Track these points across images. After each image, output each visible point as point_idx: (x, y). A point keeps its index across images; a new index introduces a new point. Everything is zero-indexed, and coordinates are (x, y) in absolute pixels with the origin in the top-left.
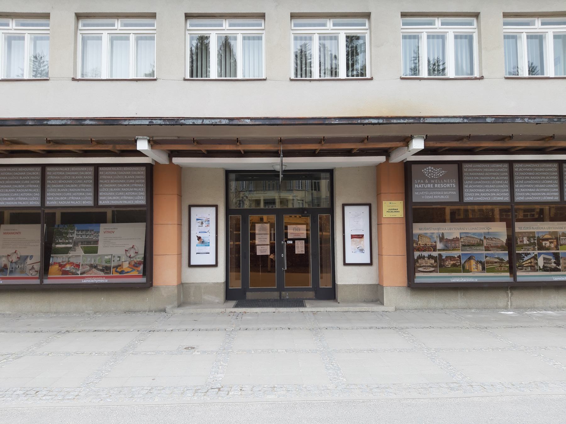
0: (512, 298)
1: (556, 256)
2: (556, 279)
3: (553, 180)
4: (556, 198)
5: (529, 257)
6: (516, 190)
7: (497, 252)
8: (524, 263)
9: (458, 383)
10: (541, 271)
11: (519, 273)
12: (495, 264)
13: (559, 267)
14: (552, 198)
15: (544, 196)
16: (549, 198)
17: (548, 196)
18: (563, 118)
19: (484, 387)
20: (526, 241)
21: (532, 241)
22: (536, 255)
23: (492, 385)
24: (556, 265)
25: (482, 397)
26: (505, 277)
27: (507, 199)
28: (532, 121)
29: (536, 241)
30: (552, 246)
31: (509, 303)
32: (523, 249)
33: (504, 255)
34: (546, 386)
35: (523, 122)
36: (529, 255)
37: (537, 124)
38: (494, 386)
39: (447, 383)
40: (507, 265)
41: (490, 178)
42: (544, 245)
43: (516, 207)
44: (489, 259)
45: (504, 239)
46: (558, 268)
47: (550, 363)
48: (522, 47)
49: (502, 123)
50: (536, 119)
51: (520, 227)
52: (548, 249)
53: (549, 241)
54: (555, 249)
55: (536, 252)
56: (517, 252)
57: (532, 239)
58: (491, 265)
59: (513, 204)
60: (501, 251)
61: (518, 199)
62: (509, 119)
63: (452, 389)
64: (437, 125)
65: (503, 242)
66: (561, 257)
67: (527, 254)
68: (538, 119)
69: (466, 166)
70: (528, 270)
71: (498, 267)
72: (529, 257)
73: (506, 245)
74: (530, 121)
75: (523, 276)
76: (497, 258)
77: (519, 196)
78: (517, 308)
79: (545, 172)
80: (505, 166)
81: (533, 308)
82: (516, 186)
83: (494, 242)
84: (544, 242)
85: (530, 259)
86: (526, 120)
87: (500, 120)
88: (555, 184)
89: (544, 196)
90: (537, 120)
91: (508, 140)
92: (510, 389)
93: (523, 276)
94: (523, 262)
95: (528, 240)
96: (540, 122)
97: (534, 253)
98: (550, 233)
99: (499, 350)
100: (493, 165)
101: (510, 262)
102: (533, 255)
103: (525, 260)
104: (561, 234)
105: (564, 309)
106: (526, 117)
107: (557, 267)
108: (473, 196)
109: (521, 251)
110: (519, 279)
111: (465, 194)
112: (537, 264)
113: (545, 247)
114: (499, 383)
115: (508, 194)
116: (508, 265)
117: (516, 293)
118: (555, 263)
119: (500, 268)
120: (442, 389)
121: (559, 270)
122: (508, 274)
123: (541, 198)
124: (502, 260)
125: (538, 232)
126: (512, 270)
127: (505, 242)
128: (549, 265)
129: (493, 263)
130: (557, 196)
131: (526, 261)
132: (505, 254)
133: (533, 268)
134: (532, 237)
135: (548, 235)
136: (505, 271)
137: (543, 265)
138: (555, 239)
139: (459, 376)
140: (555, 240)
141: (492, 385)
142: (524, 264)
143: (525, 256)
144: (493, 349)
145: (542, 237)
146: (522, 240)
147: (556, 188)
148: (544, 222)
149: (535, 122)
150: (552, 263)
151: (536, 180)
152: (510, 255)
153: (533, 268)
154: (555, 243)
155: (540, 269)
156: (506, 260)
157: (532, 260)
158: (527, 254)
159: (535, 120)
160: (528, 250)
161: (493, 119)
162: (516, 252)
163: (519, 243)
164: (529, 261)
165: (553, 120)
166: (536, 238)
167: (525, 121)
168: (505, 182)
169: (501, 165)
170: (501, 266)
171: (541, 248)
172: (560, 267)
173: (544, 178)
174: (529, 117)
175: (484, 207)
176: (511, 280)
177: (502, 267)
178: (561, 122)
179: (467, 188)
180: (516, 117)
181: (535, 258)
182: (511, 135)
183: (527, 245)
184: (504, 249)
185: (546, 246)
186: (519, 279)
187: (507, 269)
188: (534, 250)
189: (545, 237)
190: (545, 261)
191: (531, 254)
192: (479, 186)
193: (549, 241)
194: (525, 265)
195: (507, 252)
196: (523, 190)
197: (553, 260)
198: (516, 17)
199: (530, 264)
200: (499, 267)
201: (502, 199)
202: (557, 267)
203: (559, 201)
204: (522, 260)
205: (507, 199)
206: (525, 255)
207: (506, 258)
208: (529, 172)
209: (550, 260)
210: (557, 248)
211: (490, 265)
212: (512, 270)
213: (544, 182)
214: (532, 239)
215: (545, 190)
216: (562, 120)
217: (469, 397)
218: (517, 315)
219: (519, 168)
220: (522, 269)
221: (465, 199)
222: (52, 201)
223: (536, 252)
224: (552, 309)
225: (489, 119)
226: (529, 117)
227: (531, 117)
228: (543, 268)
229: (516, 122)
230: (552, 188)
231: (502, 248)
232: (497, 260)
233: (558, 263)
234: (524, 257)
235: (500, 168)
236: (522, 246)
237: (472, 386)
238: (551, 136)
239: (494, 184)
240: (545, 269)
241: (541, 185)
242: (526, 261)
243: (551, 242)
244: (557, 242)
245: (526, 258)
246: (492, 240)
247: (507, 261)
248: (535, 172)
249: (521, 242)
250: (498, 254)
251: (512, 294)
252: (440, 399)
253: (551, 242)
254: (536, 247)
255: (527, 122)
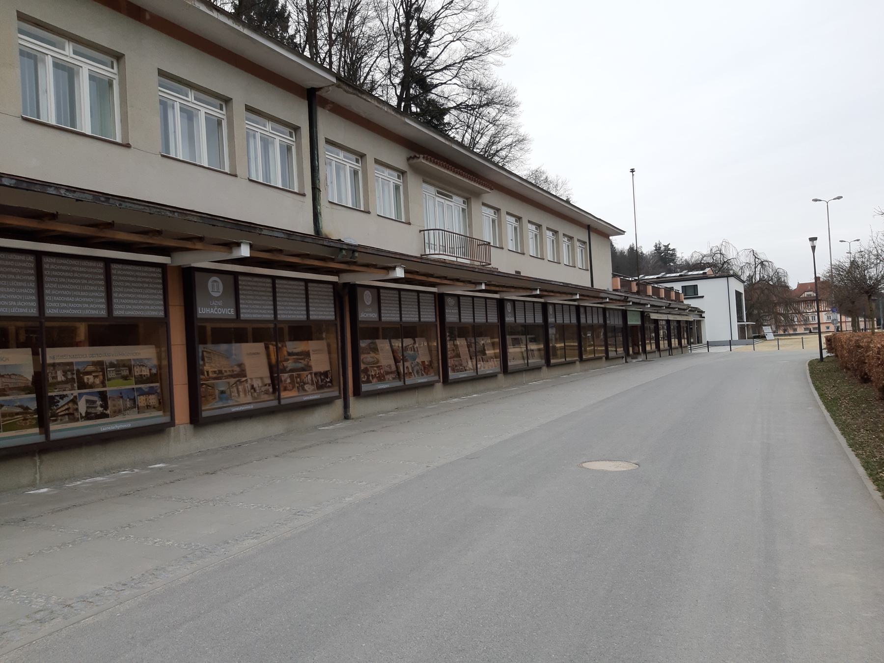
0: (41, 467)
1: (103, 396)
2: (104, 429)
3: (98, 285)
4: (32, 311)
5: (66, 400)
6: (46, 298)
7: (20, 397)
8: (59, 411)
9: (45, 610)
10: (83, 419)
11: (53, 427)
12: (16, 417)
13: (106, 412)
14: (97, 312)
15: (13, 306)
16: (21, 310)
17: (20, 307)
18: (112, 199)
19: (88, 602)
20: (60, 377)
21: (70, 377)
22: (75, 397)
23: (97, 595)
24: (102, 409)
25: (97, 614)
26: (31, 435)
27: (33, 312)
28: (70, 195)
29: (75, 376)
30: (97, 381)
31: (38, 476)
32: (56, 389)
33: (30, 401)
34: (164, 572)
35: (58, 194)
36: (67, 398)
37: (77, 200)
38: (101, 595)
39: (28, 617)
40: (35, 416)
41: (81, 282)
42: (86, 380)
43: (48, 324)
44: (6, 409)
45: (28, 373)
46: (105, 413)
47: (149, 543)
48: (46, 77)
49: (27, 190)
50: (77, 192)
51: (55, 355)
52: (91, 386)
53: (93, 374)
54: (101, 385)
55: (76, 392)
56: (50, 394)
57: (69, 373)
58: (10, 418)
59: (43, 320)
60: (26, 394)
61: (50, 312)
62: (38, 186)
63: (41, 621)
64: (50, 195)
65: (27, 380)
66: (109, 397)
67: (62, 397)
68: (79, 194)
69: (47, 260)
70: (64, 420)
71: (21, 421)
72: (66, 400)
73: (32, 384)
74: (67, 194)
75: (59, 430)
76: (19, 406)
77: (52, 308)
78: (48, 483)
79: (13, 267)
80: (100, 265)
81: (73, 477)
82: (115, 295)
83: (14, 381)
84: (86, 378)
85: (67, 403)
86: (63, 192)
87: (24, 185)
88: (31, 288)
89: (13, 306)
90: (77, 195)
91: (50, 220)
92: (125, 591)
93: (59, 430)
94: (57, 409)
95: (63, 375)
96: (82, 198)
97: (72, 394)
98: (95, 364)
99: (68, 546)
100: (12, 256)
101: (40, 411)
102: (72, 397)
103: (60, 406)
104: (108, 364)
105: (114, 471)
106: (63, 187)
107: (105, 411)
108: (57, 307)
109: (55, 392)
110: (53, 436)
111: (115, 306)
112: (77, 410)
113: (88, 383)
114: (104, 589)
115: (34, 304)
116: (37, 416)
117: (46, 457)
118: (101, 406)
119: (24, 422)
120: (24, 627)
121: (107, 416)
122: (36, 430)
123: (82, 312)
124: (27, 408)
125: (78, 363)
126: (43, 424)
127: (30, 378)
128: (93, 411)
129: (13, 416)
130: (33, 307)
131: (62, 407)
132: (32, 399)
133: (72, 416)
134: (69, 371)
135: (91, 367)
136: (31, 426)
137: (85, 411)
138: (100, 372)
139: (39, 600)
140: (101, 373)
141: (97, 595)
142: (58, 413)
143: (60, 400)
144: (59, 547)
145: (84, 370)
146: (55, 375)
147: (32, 294)
148: (78, 348)
149: (76, 197)
150: (97, 407)
151: (74, 284)
152: (40, 399)
153: (71, 417)
154: (101, 377)
155: (82, 417)
156: (33, 409)
157: (70, 405)
158: (62, 397)
159: (75, 195)
160: (64, 390)
161: (13, 182)
162: (49, 395)
163: (51, 380)
164: (66, 407)
165: (100, 199)
166: (75, 372)
167: (60, 192)
168: (31, 285)
169: (23, 257)
170: (25, 419)
171: (82, 385)
172: (108, 412)
173: (13, 277)
174: (67, 188)
175: (824, 346)
176: (41, 439)
177: (27, 419)
178: (109, 203)
179: (117, 298)
180: (47, 184)
181: (74, 401)
182: (55, 213)
183: (62, 382)
184: (29, 391)
185: (90, 383)
186: (53, 436)
187: (34, 422)
188: (73, 389)
189: (88, 369)
190: (88, 405)
191: (68, 396)
192: (66, 293)
193: (93, 374)
194: (60, 414)
195: (34, 396)
196: (123, 301)
197: (99, 403)
198: (36, 26)
199: (67, 412)
200: (23, 420)
201: (26, 310)
202: (105, 411)
203: (37, 315)
204: (56, 406)
205: (33, 312)
206: (60, 399)
207: (33, 406)
208: (129, 276)
209: (94, 402)
210: (103, 384)
211: (8, 418)
212: (43, 424)
213: (86, 288)
214: (69, 373)
215: (88, 300)
216: (111, 201)
217: (78, 622)
218: (55, 492)
219: (50, 264)
220: (55, 420)
221: (200, 312)
222: (121, 310)
223: (76, 392)
224: (98, 474)
225: (7, 179)
226: (67, 188)
227: (69, 189)
228: (86, 416)
229: (48, 192)
230: (97, 297)
231: (26, 390)
232: (19, 410)
233: (105, 406)
234: (59, 402)
235: (20, 261)
236: (55, 385)
237: (69, 606)
238: (158, 230)
239: (14, 287)
240: (88, 416)
241: (82, 293)
242: (62, 407)
243: (95, 377)
244: (104, 375)
245: (62, 403)
246: (10, 378)
247: (34, 410)
248: (74, 272)
249: (53, 378)
250: (20, 400)
251: (41, 462)
252: (34, 642)
253: (95, 377)
254: (76, 385)
255: (63, 195)
